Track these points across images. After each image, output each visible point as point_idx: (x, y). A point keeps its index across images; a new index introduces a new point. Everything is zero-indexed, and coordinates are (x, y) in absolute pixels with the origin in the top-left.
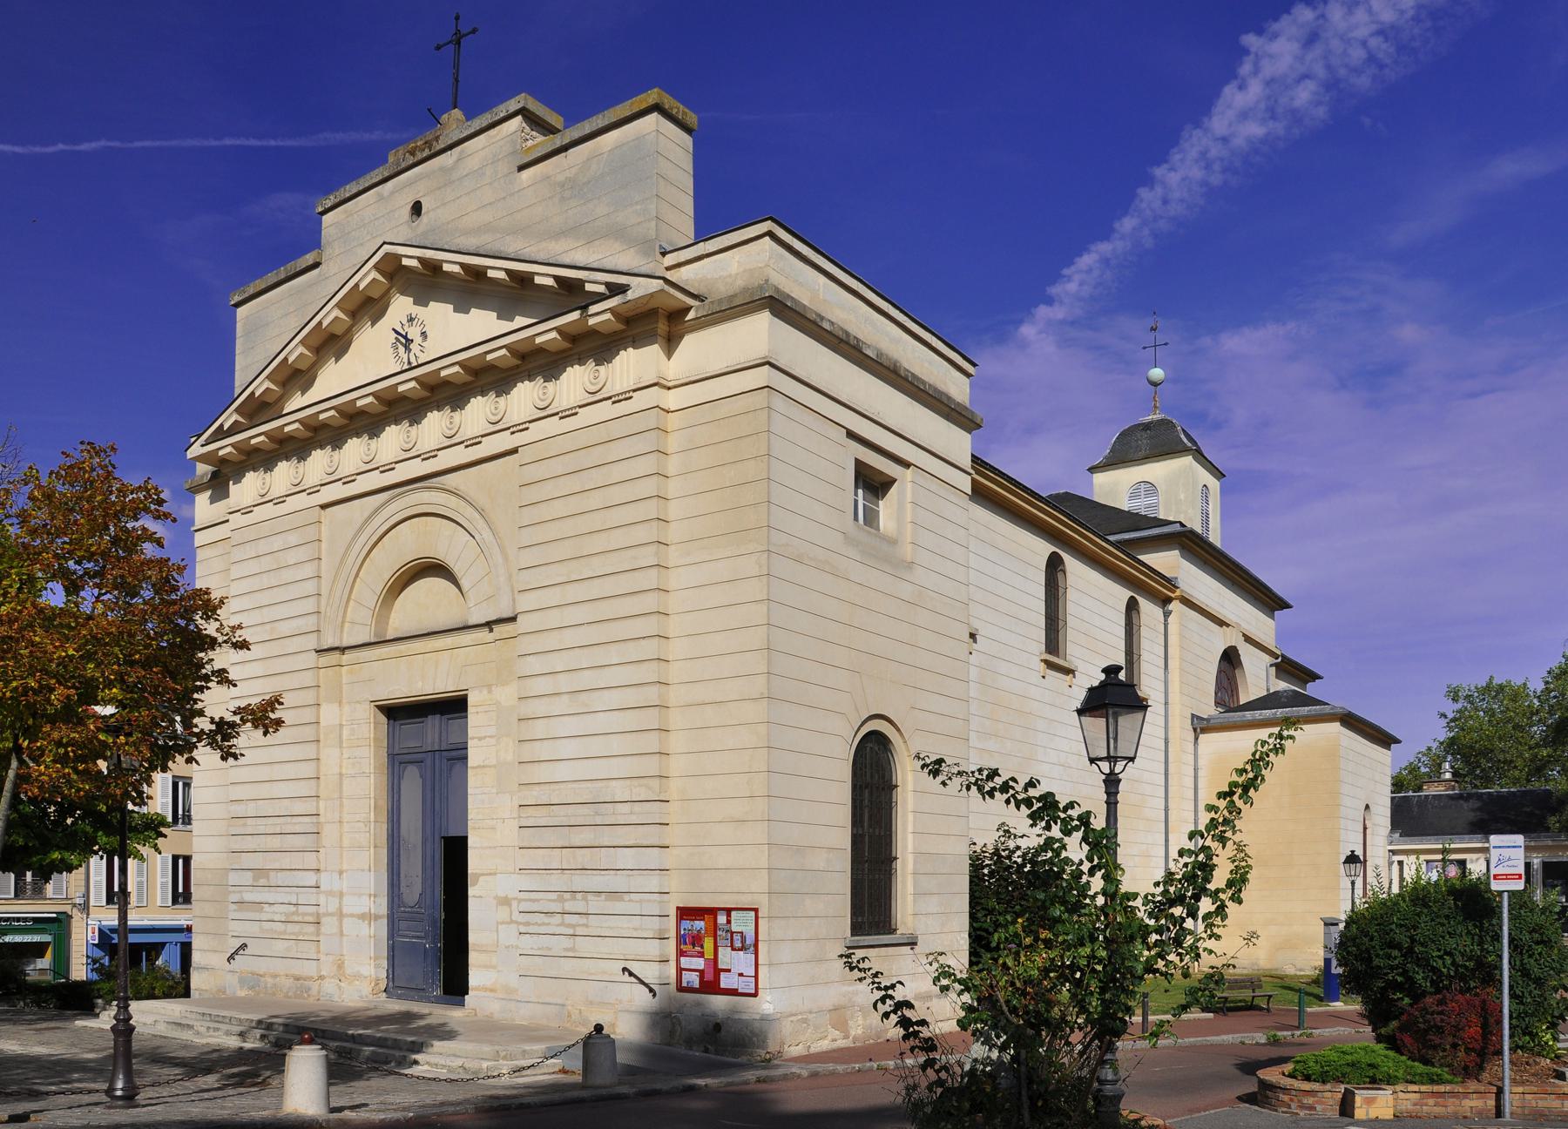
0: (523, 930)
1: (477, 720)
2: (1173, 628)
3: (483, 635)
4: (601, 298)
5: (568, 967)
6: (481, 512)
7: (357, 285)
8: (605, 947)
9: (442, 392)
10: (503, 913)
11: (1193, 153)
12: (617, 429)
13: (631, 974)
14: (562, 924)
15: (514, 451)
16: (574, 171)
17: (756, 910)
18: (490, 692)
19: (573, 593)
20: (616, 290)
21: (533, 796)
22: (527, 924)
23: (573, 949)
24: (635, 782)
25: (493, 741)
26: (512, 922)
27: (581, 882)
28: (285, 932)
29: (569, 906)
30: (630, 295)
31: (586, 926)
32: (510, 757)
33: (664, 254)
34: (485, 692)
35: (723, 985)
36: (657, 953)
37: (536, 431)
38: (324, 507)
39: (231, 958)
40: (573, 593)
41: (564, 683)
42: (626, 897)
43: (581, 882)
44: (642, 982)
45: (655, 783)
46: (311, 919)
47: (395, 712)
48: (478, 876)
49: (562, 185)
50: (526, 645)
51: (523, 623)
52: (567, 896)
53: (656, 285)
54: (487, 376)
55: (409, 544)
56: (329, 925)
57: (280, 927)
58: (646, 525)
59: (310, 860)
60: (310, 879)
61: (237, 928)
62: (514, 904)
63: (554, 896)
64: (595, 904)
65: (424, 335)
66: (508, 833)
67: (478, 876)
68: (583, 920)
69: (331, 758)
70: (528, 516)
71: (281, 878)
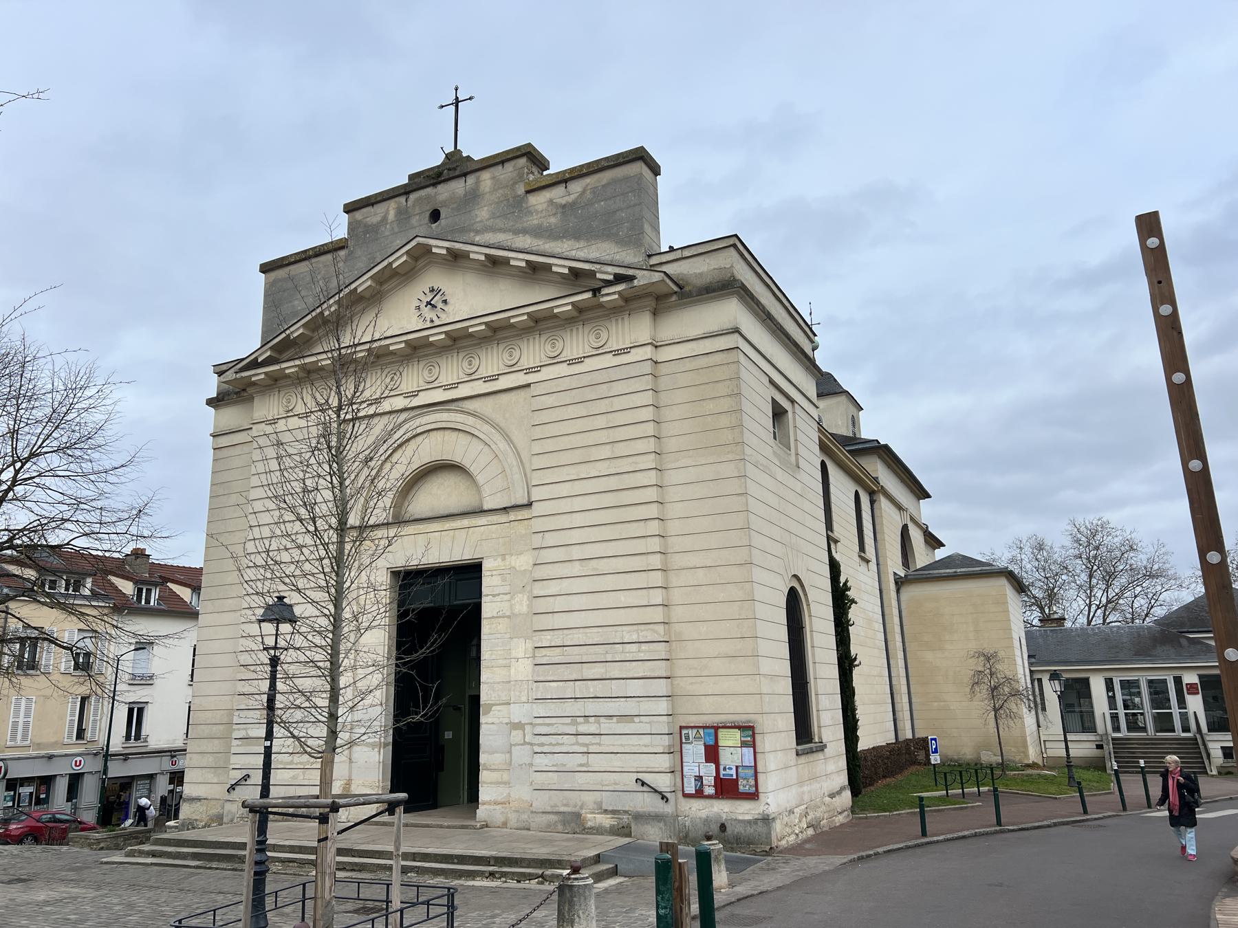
0: (537, 749)
1: (490, 582)
2: (673, 466)
3: (502, 518)
4: (608, 283)
5: (582, 780)
6: (496, 426)
7: (391, 264)
8: (617, 762)
9: (459, 341)
10: (517, 736)
13: (643, 784)
14: (577, 743)
15: (528, 385)
17: (681, 728)
18: (504, 559)
19: (579, 488)
20: (619, 279)
21: (547, 639)
22: (542, 745)
23: (587, 765)
24: (642, 627)
25: (508, 597)
26: (525, 743)
27: (592, 708)
28: (292, 762)
29: (582, 729)
30: (636, 282)
31: (599, 744)
32: (525, 609)
33: (649, 256)
34: (499, 559)
35: (741, 788)
36: (667, 765)
37: (546, 373)
39: (233, 787)
40: (579, 488)
41: (577, 553)
42: (636, 719)
43: (592, 708)
44: (656, 791)
45: (660, 628)
49: (564, 206)
50: (539, 525)
51: (537, 509)
52: (581, 720)
53: (657, 277)
54: (499, 332)
58: (645, 440)
61: (236, 761)
62: (528, 728)
63: (569, 720)
64: (606, 726)
65: (445, 302)
66: (523, 669)
68: (596, 739)
70: (538, 432)
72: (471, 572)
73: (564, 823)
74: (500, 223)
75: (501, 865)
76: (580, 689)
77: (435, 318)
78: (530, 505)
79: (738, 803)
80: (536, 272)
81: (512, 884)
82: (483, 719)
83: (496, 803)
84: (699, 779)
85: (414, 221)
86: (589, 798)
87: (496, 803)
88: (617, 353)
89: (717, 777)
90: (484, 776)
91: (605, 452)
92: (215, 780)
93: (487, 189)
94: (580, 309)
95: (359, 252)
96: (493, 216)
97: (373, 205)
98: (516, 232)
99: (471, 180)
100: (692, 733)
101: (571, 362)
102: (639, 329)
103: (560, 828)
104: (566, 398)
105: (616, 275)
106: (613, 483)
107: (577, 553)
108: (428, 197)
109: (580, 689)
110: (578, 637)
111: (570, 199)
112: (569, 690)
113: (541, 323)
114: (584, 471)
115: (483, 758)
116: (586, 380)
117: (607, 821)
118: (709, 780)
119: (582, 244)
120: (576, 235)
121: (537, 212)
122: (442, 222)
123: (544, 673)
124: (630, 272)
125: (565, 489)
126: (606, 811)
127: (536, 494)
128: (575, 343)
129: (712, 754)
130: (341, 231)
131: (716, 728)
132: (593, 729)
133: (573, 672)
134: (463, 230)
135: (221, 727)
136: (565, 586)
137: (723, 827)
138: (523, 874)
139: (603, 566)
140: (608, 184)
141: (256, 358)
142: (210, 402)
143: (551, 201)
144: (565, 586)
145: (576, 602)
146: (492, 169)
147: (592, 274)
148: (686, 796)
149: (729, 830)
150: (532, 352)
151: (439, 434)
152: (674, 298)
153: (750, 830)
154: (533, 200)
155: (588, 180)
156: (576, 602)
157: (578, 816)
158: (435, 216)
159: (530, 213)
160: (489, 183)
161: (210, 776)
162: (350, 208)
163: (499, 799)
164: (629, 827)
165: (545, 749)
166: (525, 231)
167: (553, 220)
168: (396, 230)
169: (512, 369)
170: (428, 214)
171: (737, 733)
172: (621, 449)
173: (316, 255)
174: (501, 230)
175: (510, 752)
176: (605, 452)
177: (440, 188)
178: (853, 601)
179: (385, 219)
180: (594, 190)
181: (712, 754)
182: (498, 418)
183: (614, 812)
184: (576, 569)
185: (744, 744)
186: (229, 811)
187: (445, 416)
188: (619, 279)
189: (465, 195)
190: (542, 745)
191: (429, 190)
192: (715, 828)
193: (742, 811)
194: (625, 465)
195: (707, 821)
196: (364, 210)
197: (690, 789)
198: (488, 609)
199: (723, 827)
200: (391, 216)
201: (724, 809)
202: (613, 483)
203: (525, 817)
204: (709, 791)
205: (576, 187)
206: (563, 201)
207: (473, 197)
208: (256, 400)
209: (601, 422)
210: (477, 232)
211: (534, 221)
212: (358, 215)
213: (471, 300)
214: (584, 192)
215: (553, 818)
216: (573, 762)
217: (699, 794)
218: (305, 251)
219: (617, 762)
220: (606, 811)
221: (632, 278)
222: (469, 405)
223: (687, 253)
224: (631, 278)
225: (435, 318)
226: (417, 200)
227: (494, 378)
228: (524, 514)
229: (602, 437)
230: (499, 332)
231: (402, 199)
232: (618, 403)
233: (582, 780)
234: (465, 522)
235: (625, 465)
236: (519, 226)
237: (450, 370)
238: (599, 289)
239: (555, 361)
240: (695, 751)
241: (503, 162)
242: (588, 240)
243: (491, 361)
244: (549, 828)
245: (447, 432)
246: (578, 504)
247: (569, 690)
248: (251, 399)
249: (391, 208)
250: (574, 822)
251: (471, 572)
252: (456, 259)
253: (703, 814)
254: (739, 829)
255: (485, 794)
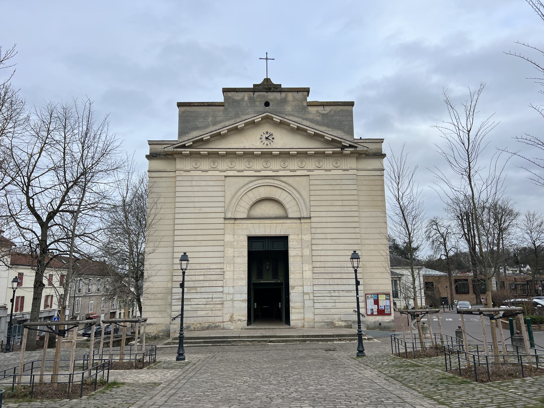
4: (347, 147)
5: (333, 311)
8: (346, 305)
11: (51, 273)
12: (343, 177)
14: (331, 299)
16: (252, 141)
20: (351, 146)
22: (318, 300)
23: (335, 306)
27: (336, 288)
28: (205, 308)
29: (333, 294)
35: (386, 312)
37: (316, 172)
38: (225, 176)
41: (329, 236)
43: (336, 288)
46: (220, 303)
47: (180, 105)
48: (294, 287)
49: (323, 114)
51: (313, 220)
54: (302, 155)
55: (264, 192)
56: (227, 304)
57: (204, 306)
59: (220, 283)
60: (220, 289)
63: (328, 292)
64: (342, 294)
67: (243, 301)
68: (339, 298)
69: (230, 252)
71: (199, 290)
72: (285, 239)
73: (328, 325)
74: (296, 114)
75: (304, 339)
76: (331, 281)
77: (269, 144)
78: (310, 218)
79: (384, 317)
80: (316, 136)
81: (348, 342)
82: (291, 291)
83: (298, 320)
84: (372, 310)
85: (257, 103)
86: (336, 317)
87: (298, 320)
88: (344, 170)
89: (378, 309)
90: (292, 311)
91: (340, 203)
92: (160, 316)
93: (291, 100)
94: (334, 153)
95: (230, 110)
96: (293, 110)
97: (237, 92)
98: (304, 119)
99: (283, 94)
100: (369, 296)
101: (326, 170)
102: (352, 163)
103: (326, 327)
104: (324, 182)
105: (350, 145)
106: (342, 214)
107: (329, 236)
108: (264, 96)
109: (331, 281)
110: (330, 264)
111: (325, 112)
112: (328, 282)
113: (319, 155)
114: (331, 209)
115: (291, 305)
116: (331, 177)
117: (343, 324)
118: (375, 310)
119: (330, 129)
120: (328, 126)
121: (312, 114)
122: (271, 107)
123: (316, 276)
124: (356, 145)
125: (324, 214)
126: (342, 321)
127: (313, 214)
128: (328, 164)
129: (376, 302)
130: (220, 98)
131: (378, 294)
132: (337, 294)
133: (329, 276)
134: (280, 113)
135: (162, 295)
136: (325, 247)
137: (380, 324)
138: (352, 339)
139: (339, 241)
140: (340, 111)
141: (185, 144)
142: (147, 157)
143: (317, 111)
144: (325, 247)
145: (329, 253)
146: (293, 93)
147: (341, 142)
148: (368, 315)
149: (382, 325)
150: (311, 164)
151: (269, 188)
152: (364, 155)
153: (389, 324)
154: (310, 109)
155: (332, 107)
156: (329, 253)
157: (332, 323)
158: (267, 104)
159: (309, 113)
160: (291, 98)
161: (157, 315)
162: (225, 90)
163: (299, 318)
164: (351, 325)
165: (319, 301)
166: (307, 119)
167: (318, 118)
168: (249, 105)
169: (302, 169)
170: (264, 103)
171: (384, 296)
172: (346, 203)
173: (208, 106)
174: (298, 117)
175: (304, 303)
176: (340, 203)
177: (269, 93)
178: (402, 255)
179: (243, 99)
180: (335, 111)
181: (376, 302)
182: (295, 186)
183: (345, 321)
184: (329, 242)
185: (387, 299)
186: (173, 328)
187: (272, 181)
188: (351, 146)
189: (281, 99)
190: (318, 300)
191: (264, 93)
192: (378, 324)
193: (46, 344)
194: (347, 209)
195: (375, 322)
196: (233, 93)
197: (369, 313)
198: (291, 253)
199: (380, 324)
200: (246, 98)
201: (380, 318)
202: (342, 214)
203: (311, 324)
204: (376, 313)
205: (328, 109)
206: (323, 112)
207: (284, 101)
208: (177, 161)
209: (338, 193)
210: (286, 115)
211: (311, 116)
212: (230, 94)
213: (283, 141)
214: (331, 111)
215: (324, 324)
216: (330, 305)
217: (372, 314)
218: (203, 103)
219: (346, 305)
220: (342, 321)
221: (356, 147)
222: (282, 179)
223: (367, 141)
224: (356, 147)
225: (269, 144)
226: (258, 96)
227: (294, 171)
228: (308, 221)
229: (339, 198)
230: (302, 155)
231: (252, 94)
232: (344, 187)
233: (333, 311)
234: (281, 221)
235: (347, 209)
236: (304, 117)
237: (275, 165)
238: (344, 149)
239: (319, 169)
240: (371, 302)
241: (298, 92)
242: (332, 129)
243: (293, 164)
244: (322, 327)
245: (272, 187)
246: (329, 220)
247: (328, 282)
248: (175, 159)
249: (246, 96)
250: (331, 325)
251: (285, 239)
252: (282, 124)
253: (373, 320)
254: (385, 324)
255: (292, 317)
